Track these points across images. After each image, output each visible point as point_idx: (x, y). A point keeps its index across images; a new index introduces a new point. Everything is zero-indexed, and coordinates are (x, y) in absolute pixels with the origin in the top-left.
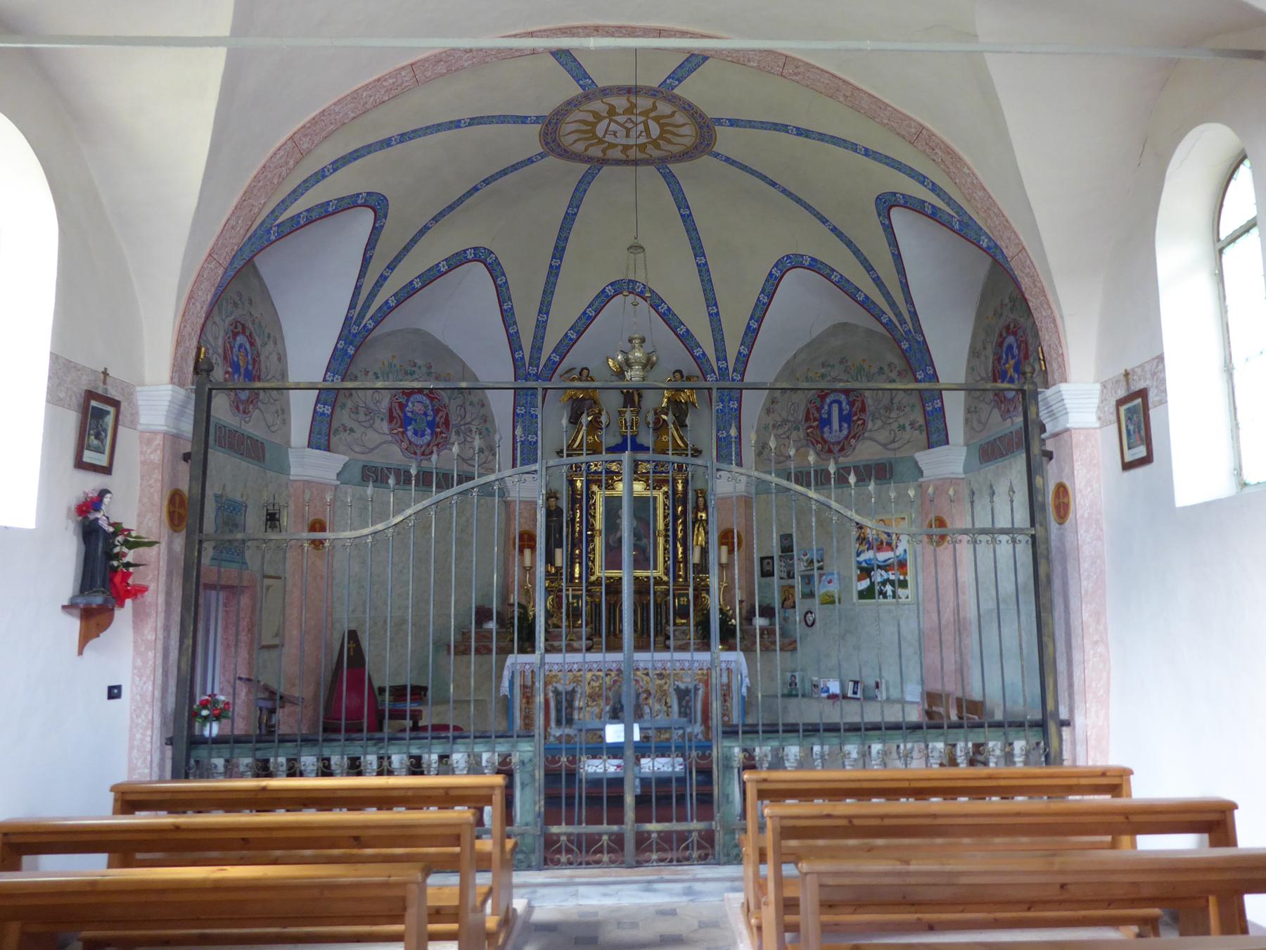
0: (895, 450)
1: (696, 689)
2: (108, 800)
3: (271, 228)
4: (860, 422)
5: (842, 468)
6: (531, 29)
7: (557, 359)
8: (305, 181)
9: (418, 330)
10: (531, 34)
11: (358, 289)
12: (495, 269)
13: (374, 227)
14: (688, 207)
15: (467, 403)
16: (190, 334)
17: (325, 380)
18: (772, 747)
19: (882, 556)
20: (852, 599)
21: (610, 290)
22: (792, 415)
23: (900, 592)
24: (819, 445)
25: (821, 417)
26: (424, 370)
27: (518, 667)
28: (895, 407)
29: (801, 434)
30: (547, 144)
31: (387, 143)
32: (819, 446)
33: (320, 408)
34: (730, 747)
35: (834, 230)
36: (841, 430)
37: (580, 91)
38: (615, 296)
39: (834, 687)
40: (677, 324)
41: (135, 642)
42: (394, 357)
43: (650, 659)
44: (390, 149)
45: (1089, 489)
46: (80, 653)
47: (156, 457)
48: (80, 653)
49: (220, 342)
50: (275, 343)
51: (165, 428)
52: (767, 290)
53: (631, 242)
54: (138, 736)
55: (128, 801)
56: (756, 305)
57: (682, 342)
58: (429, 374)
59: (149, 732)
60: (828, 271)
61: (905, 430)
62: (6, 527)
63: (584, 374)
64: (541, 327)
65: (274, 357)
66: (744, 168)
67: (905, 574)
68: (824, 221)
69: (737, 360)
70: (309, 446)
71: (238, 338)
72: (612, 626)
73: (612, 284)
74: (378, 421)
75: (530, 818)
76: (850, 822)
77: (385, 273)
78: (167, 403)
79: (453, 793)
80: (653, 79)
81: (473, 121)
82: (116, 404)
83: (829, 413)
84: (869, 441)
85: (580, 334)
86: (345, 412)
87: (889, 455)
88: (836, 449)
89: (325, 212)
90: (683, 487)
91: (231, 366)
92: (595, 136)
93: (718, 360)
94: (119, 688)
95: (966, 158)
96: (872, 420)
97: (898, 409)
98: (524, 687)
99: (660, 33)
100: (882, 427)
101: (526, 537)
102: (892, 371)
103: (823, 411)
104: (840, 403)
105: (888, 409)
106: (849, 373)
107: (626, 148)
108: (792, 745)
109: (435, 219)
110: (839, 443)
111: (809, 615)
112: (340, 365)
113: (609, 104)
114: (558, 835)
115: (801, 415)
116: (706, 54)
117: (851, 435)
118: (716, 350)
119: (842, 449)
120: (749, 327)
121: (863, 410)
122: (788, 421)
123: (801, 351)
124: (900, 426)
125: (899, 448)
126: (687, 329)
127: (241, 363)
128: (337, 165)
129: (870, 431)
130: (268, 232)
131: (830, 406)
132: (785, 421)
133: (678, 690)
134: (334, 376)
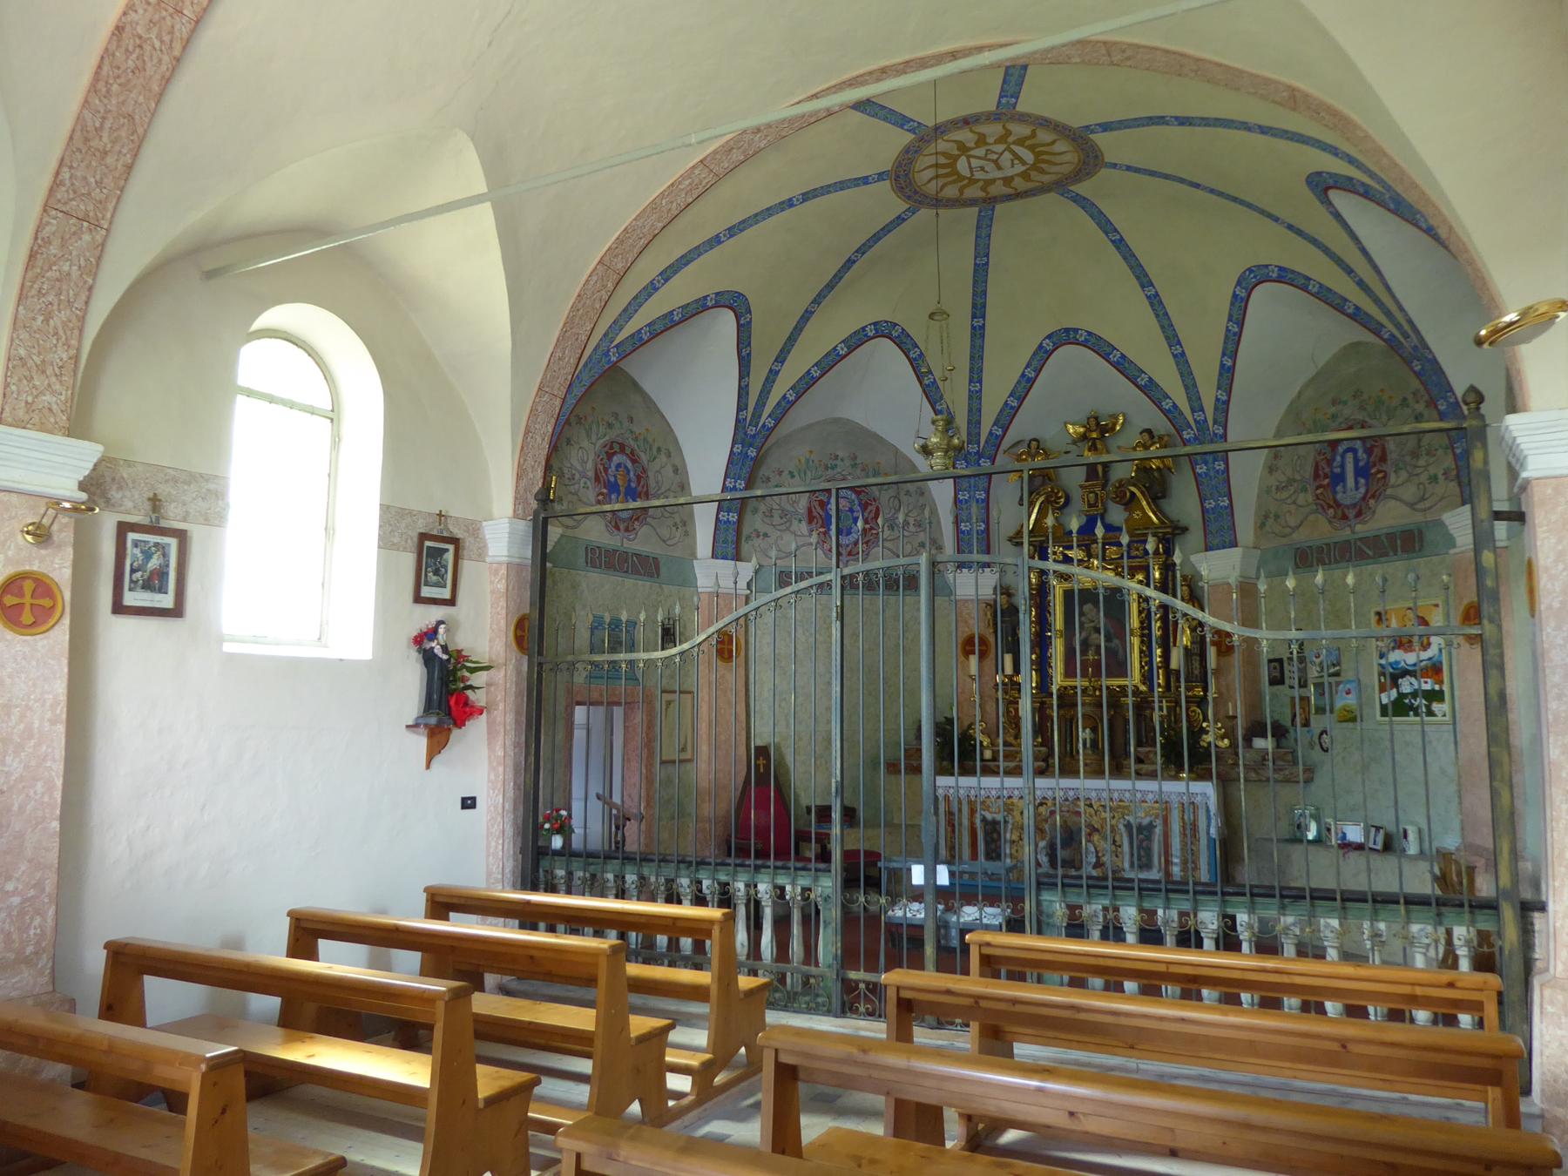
0: (1425, 510)
1: (1151, 826)
2: (421, 901)
3: (609, 351)
4: (1380, 476)
5: (1360, 539)
6: (814, 92)
7: (1000, 432)
8: (635, 298)
9: (840, 419)
10: (815, 96)
11: (743, 391)
12: (904, 342)
13: (739, 326)
14: (1116, 230)
15: (902, 493)
16: (533, 467)
17: (724, 489)
18: (1102, 905)
19: (1410, 658)
20: (1375, 716)
21: (1048, 345)
22: (1299, 472)
23: (1436, 707)
24: (1332, 511)
25: (1332, 472)
26: (848, 463)
27: (962, 791)
28: (1424, 453)
29: (1310, 498)
30: (909, 198)
31: (716, 241)
32: (1331, 511)
33: (724, 516)
34: (1051, 901)
35: (1290, 227)
36: (1357, 488)
37: (910, 136)
38: (1055, 350)
39: (1355, 834)
40: (1137, 374)
41: (489, 757)
42: (811, 452)
43: (1131, 788)
44: (721, 246)
45: (1561, 567)
46: (428, 767)
47: (502, 586)
48: (428, 767)
49: (590, 465)
50: (669, 455)
51: (518, 560)
52: (1235, 317)
53: (932, 308)
54: (493, 844)
55: (441, 903)
56: (1226, 337)
57: (1145, 394)
58: (854, 466)
59: (501, 842)
60: (1303, 281)
61: (1437, 483)
62: (341, 660)
63: (1036, 447)
64: (975, 397)
65: (669, 469)
66: (1152, 173)
67: (1441, 682)
68: (1276, 220)
69: (1216, 409)
70: (714, 556)
71: (615, 458)
72: (1068, 746)
73: (1049, 337)
74: (795, 523)
75: (830, 960)
76: (977, 1003)
77: (773, 367)
78: (507, 535)
79: (679, 924)
80: (987, 101)
81: (806, 197)
82: (455, 541)
83: (1342, 466)
84: (1393, 501)
85: (1022, 400)
86: (759, 516)
87: (1419, 518)
88: (1351, 513)
89: (669, 323)
90: (1161, 574)
91: (605, 487)
92: (961, 178)
93: (1193, 411)
94: (473, 799)
95: (1354, 116)
96: (1395, 472)
97: (1427, 455)
98: (950, 814)
99: (954, 55)
100: (1407, 481)
101: (726, 655)
102: (1417, 402)
103: (1335, 464)
104: (1354, 451)
105: (1415, 454)
106: (1365, 409)
107: (1007, 181)
108: (1129, 905)
109: (817, 300)
110: (1354, 505)
111: (1325, 736)
112: (741, 469)
113: (979, 133)
114: (857, 982)
115: (1309, 471)
116: (1022, 62)
117: (1369, 495)
118: (1189, 399)
119: (1359, 514)
120: (1222, 366)
121: (1383, 458)
122: (1295, 481)
123: (1306, 386)
124: (1430, 478)
125: (1430, 508)
126: (1150, 378)
127: (620, 482)
128: (667, 274)
129: (1392, 487)
130: (607, 354)
131: (1343, 457)
132: (1291, 481)
133: (1128, 826)
134: (735, 482)
